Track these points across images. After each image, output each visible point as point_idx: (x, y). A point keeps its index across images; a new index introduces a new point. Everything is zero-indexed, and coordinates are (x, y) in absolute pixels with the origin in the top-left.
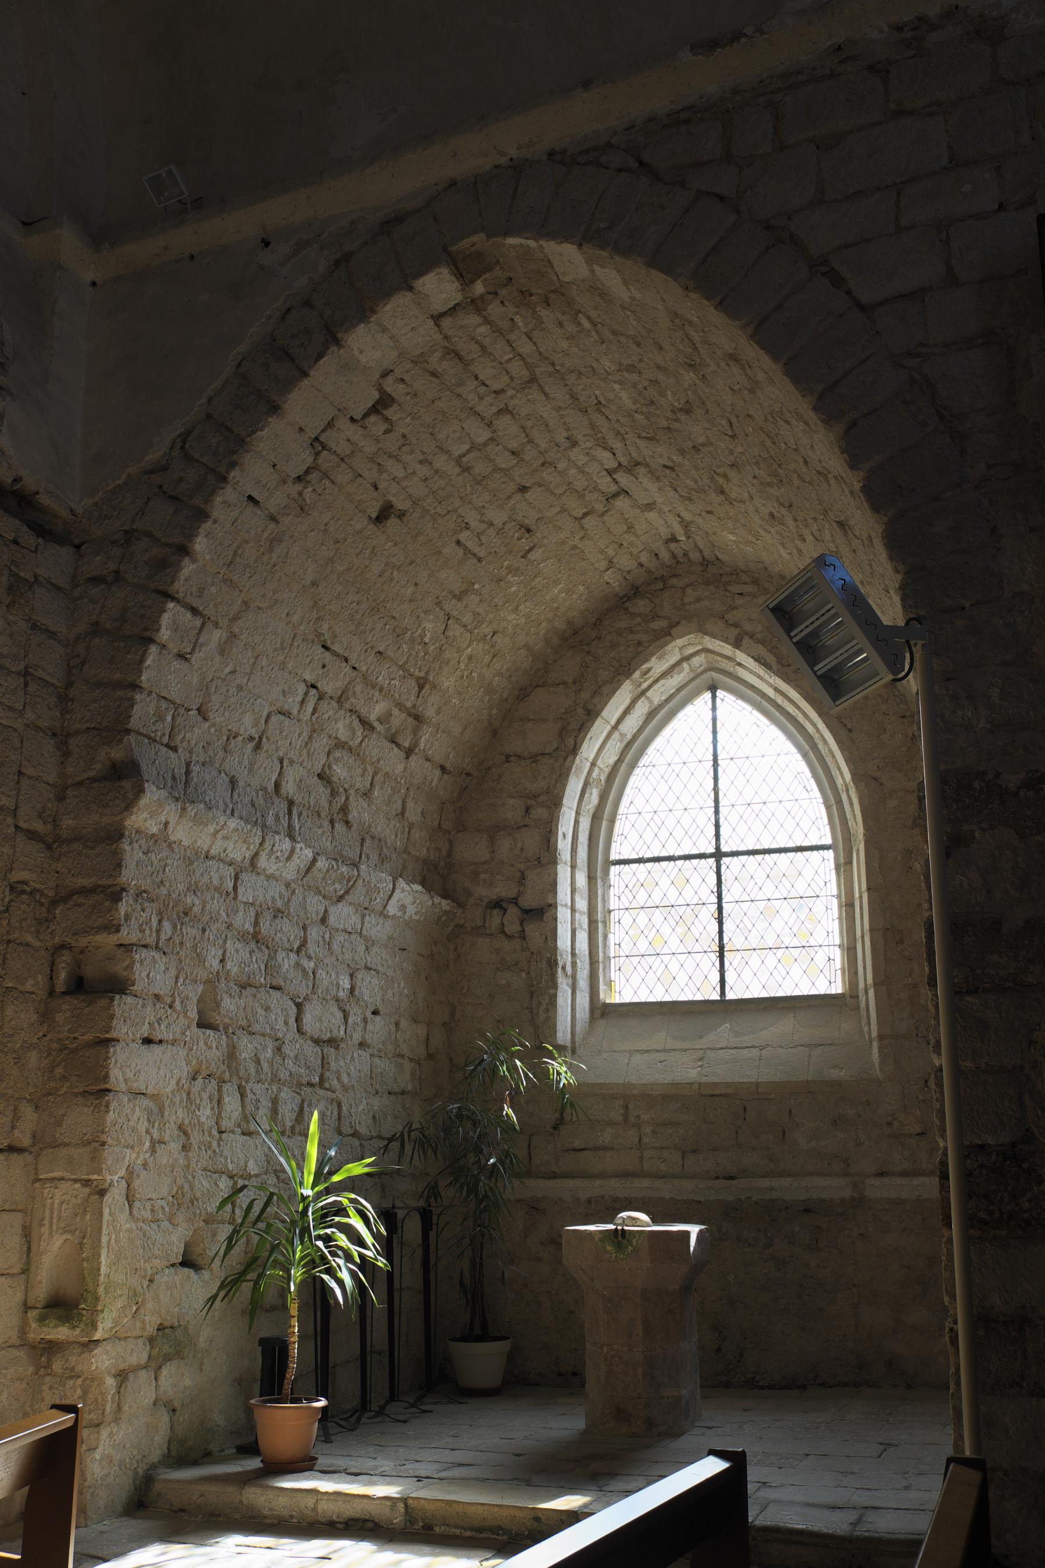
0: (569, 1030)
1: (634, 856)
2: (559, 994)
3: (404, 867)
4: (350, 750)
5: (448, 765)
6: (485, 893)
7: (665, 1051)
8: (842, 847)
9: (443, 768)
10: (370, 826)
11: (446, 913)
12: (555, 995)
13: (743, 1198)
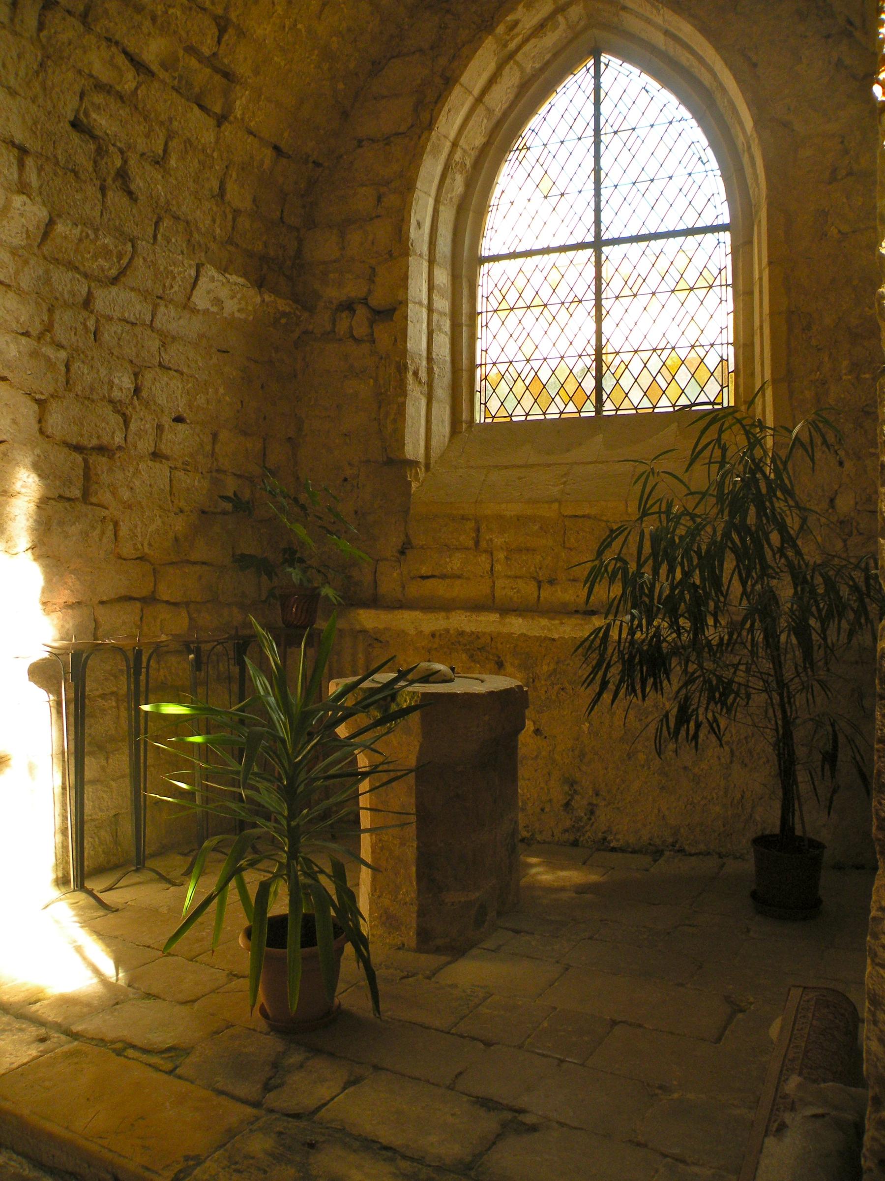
0: (422, 443)
1: (505, 251)
2: (409, 403)
3: (230, 261)
4: (121, 97)
5: (283, 145)
6: (333, 294)
7: (526, 466)
8: (741, 229)
9: (276, 148)
10: (168, 203)
11: (284, 314)
12: (404, 403)
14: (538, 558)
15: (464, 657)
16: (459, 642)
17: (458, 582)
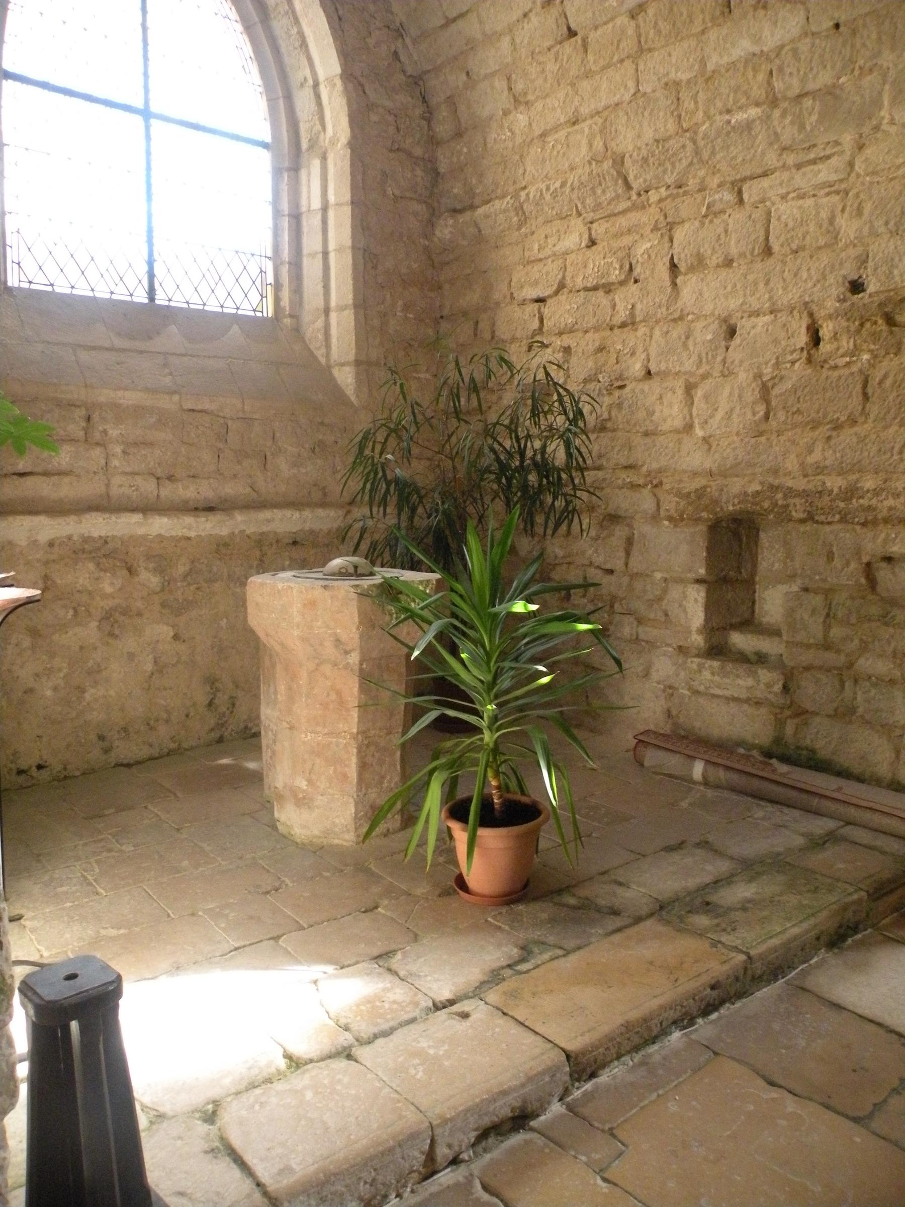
13: (236, 531)
14: (157, 452)
15: (91, 566)
16: (83, 551)
17: (66, 480)
